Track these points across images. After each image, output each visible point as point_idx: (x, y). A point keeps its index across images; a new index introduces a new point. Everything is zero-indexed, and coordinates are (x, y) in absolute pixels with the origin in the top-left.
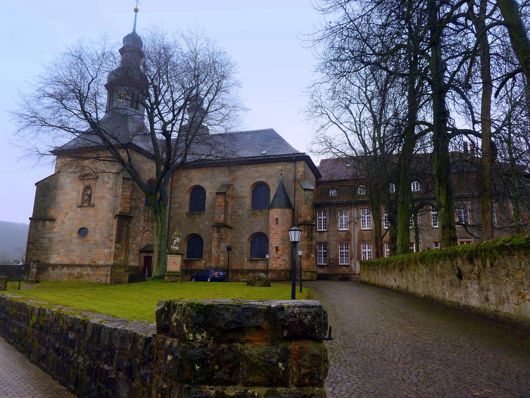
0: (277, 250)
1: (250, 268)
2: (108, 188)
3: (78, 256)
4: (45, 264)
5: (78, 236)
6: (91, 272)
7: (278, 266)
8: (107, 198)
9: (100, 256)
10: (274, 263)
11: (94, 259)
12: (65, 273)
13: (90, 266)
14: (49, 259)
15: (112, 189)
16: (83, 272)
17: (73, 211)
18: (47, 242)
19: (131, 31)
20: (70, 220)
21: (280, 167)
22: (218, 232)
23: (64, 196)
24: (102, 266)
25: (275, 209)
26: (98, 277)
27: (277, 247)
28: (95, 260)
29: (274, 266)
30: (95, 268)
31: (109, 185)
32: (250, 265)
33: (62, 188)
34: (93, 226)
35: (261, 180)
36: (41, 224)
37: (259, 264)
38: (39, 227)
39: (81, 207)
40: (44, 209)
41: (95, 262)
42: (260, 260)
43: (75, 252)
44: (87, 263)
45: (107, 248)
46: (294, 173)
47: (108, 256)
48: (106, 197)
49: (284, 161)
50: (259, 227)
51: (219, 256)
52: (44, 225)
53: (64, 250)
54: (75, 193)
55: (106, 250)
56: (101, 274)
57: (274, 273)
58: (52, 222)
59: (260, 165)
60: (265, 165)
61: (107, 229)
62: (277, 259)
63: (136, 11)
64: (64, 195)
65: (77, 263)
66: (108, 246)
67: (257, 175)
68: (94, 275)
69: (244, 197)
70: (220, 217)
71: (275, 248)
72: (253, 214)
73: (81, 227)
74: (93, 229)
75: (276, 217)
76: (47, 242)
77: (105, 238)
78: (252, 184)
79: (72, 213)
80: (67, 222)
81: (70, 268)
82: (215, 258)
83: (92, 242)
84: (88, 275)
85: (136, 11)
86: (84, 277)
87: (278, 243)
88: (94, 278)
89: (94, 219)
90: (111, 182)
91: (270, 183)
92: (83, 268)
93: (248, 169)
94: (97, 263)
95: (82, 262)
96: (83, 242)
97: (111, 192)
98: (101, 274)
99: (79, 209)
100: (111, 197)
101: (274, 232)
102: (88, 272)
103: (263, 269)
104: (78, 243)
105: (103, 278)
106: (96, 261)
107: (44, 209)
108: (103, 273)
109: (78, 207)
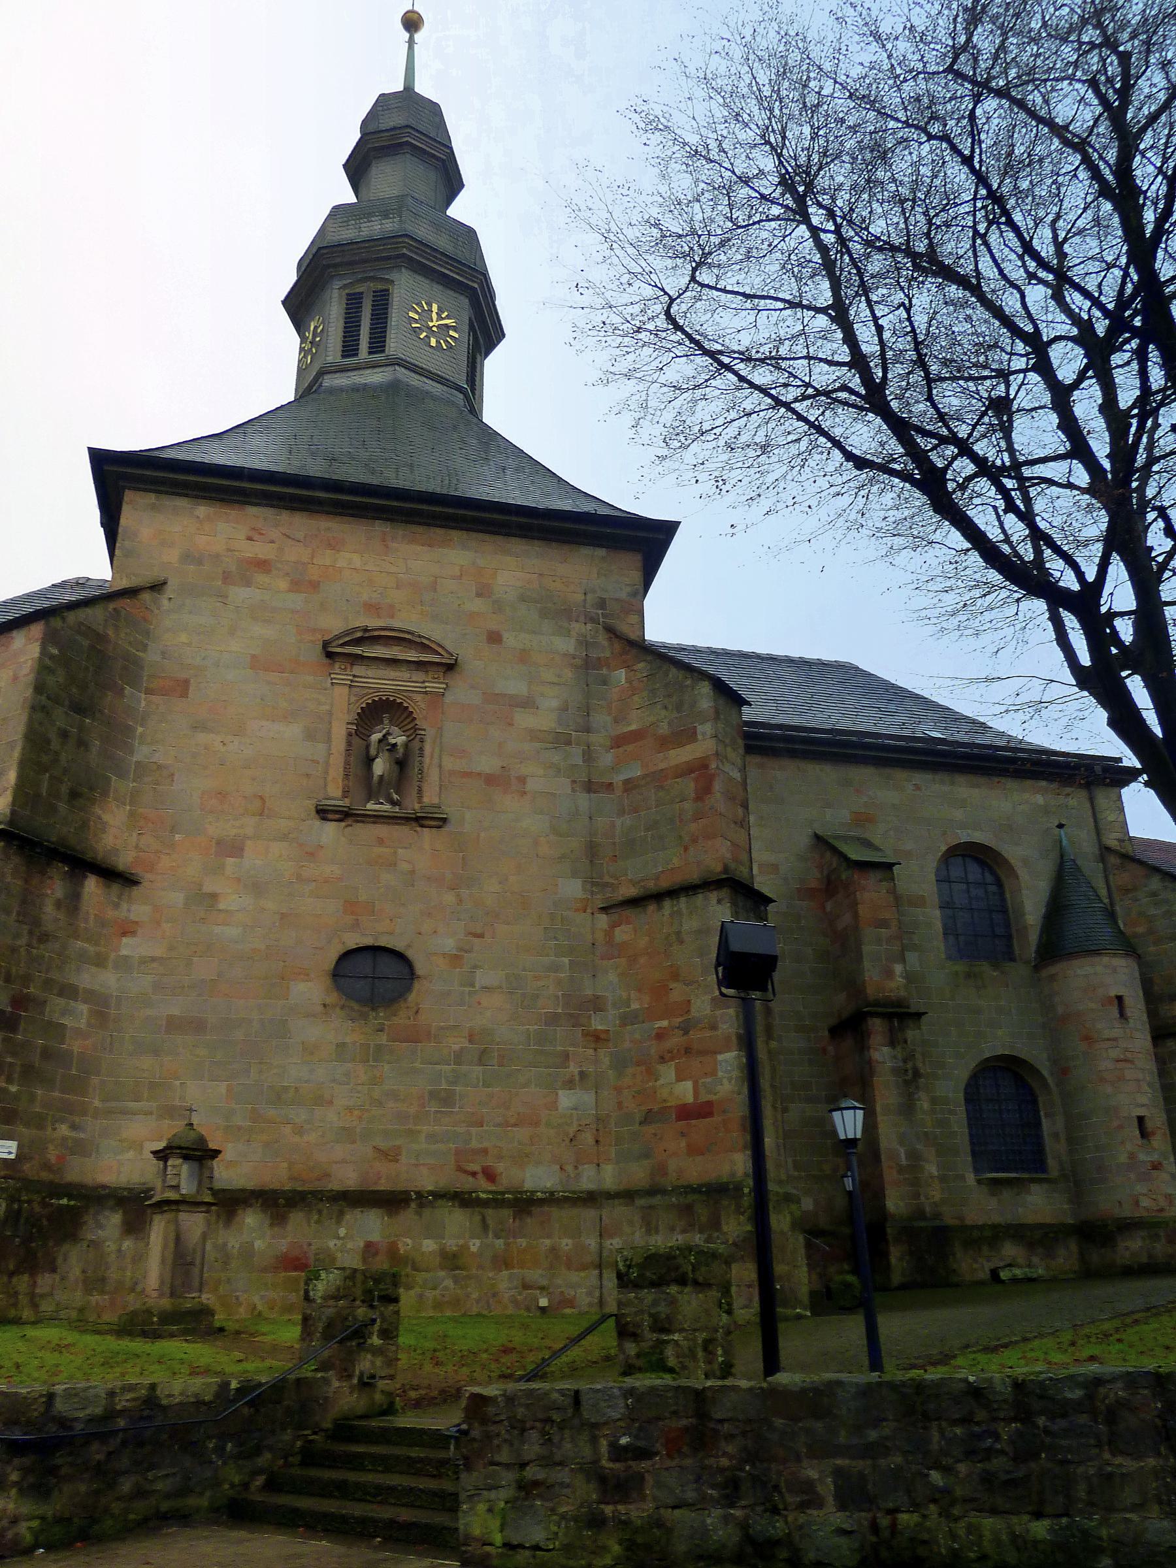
0: (1144, 1134)
1: (997, 1219)
2: (534, 735)
3: (347, 1134)
4: (69, 1190)
5: (333, 998)
6: (475, 1245)
7: (1162, 1203)
8: (531, 785)
9: (522, 1133)
10: (1140, 1188)
11: (485, 1151)
12: (247, 1252)
13: (463, 1200)
14: (80, 1148)
15: (561, 740)
16: (405, 1245)
17: (284, 837)
18: (82, 1024)
19: (399, 87)
20: (257, 888)
21: (1040, 799)
22: (892, 1044)
23: (202, 738)
24: (551, 1199)
25: (1105, 959)
26: (535, 1275)
27: (1141, 1120)
28: (490, 1162)
29: (1145, 1202)
30: (506, 1213)
31: (544, 719)
32: (993, 1203)
33: (182, 688)
34: (449, 944)
35: (978, 837)
36: (55, 887)
37: (1029, 1198)
38: (49, 909)
39: (345, 815)
40: (74, 795)
41: (490, 1176)
42: (1033, 1180)
43: (320, 1101)
44: (427, 1182)
45: (570, 1084)
46: (1092, 824)
47: (588, 1137)
48: (522, 780)
49: (1050, 778)
50: (1000, 1033)
51: (914, 1156)
52: (72, 905)
53: (222, 1088)
54: (293, 731)
55: (566, 1099)
56: (553, 1249)
57: (1156, 1237)
58: (116, 888)
59: (961, 779)
60: (982, 780)
61: (556, 968)
62: (1155, 1173)
63: (412, 23)
64: (199, 726)
65: (348, 1178)
66: (573, 1069)
67: (958, 814)
68: (502, 1262)
69: (920, 902)
70: (889, 974)
71: (1136, 1123)
72: (968, 976)
73: (354, 940)
74: (455, 959)
75: (1113, 993)
76: (82, 1024)
77: (553, 1019)
78: (944, 848)
79: (277, 848)
80: (233, 900)
81: (296, 1218)
82: (901, 1170)
83: (456, 1043)
84: (452, 1261)
85: (412, 23)
86: (420, 1277)
87: (1144, 1100)
88: (504, 1282)
89: (449, 898)
90: (550, 701)
91: (1013, 852)
92: (408, 1216)
93: (917, 787)
94: (504, 1183)
95: (385, 1178)
96: (383, 1039)
97: (556, 758)
98: (553, 1249)
99: (330, 831)
100: (563, 785)
101: (1114, 1054)
102: (452, 1244)
103: (1048, 1220)
104: (341, 1046)
105: (574, 1277)
106: (500, 1167)
107: (74, 795)
108: (566, 1244)
109: (323, 813)
